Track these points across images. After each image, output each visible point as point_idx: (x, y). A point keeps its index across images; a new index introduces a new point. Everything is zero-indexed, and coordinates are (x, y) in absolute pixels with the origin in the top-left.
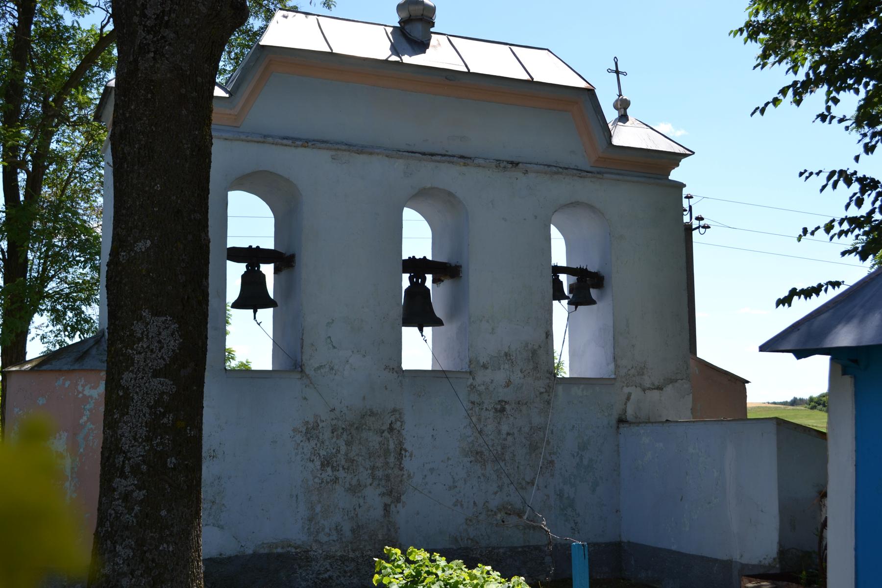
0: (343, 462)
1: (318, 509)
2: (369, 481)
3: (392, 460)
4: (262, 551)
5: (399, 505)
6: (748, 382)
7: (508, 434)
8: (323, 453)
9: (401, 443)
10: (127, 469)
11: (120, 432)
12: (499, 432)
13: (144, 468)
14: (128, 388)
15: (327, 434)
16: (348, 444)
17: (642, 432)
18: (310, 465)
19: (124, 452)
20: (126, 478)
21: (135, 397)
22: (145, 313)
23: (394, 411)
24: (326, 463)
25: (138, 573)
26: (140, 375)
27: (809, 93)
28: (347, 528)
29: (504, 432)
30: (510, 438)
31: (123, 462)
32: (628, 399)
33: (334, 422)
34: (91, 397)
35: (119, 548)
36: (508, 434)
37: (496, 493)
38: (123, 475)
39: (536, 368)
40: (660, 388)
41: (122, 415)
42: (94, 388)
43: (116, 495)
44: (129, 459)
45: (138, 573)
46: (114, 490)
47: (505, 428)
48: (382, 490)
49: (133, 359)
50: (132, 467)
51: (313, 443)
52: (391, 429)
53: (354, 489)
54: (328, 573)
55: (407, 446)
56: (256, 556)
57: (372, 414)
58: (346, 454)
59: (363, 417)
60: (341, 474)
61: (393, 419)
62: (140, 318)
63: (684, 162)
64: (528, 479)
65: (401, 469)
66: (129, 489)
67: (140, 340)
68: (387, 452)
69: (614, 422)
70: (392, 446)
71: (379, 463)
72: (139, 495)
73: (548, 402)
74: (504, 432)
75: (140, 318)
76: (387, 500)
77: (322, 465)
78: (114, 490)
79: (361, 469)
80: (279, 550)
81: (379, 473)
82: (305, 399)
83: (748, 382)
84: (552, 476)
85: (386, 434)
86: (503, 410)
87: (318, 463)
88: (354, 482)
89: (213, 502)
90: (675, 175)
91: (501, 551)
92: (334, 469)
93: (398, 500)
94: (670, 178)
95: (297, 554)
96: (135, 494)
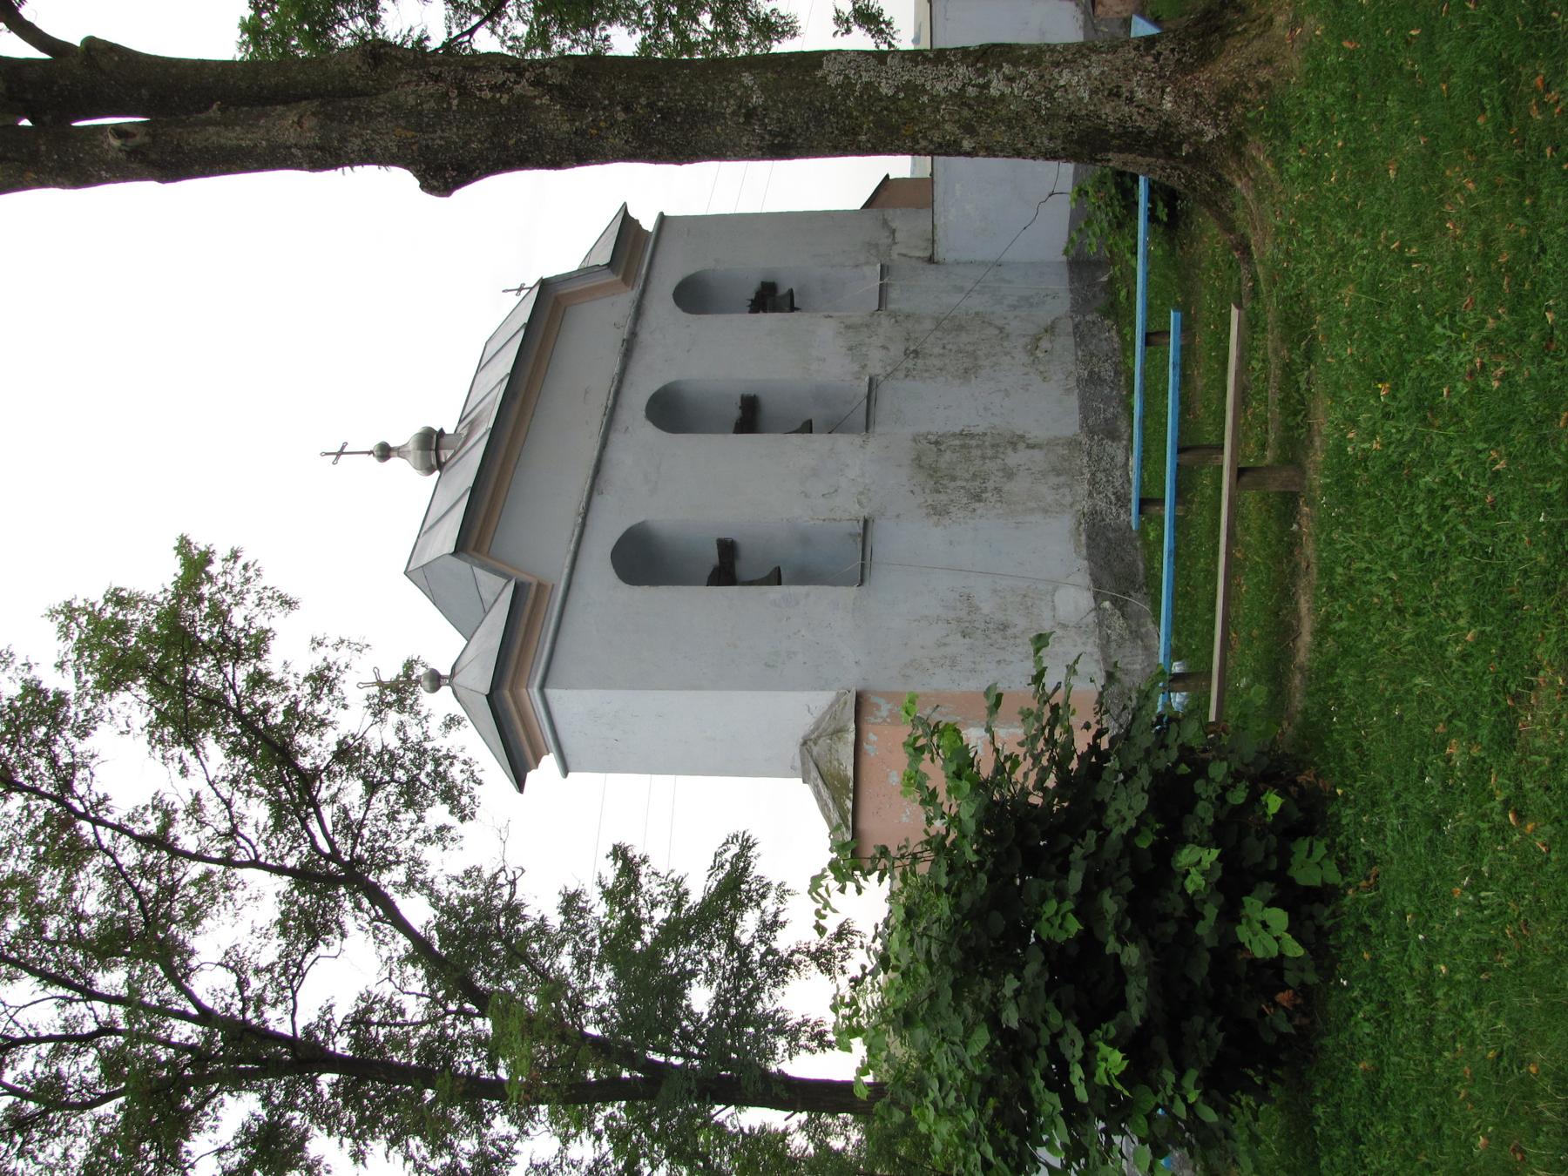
0: (977, 483)
1: (1033, 505)
2: (999, 461)
3: (973, 443)
4: (1084, 552)
5: (1027, 436)
6: (887, 176)
7: (944, 348)
8: (965, 500)
9: (954, 435)
10: (981, 81)
11: (942, 94)
12: (942, 355)
13: (979, 65)
14: (897, 87)
15: (943, 497)
16: (953, 479)
17: (943, 220)
18: (979, 512)
19: (964, 86)
20: (990, 82)
21: (906, 78)
22: (819, 74)
23: (914, 440)
24: (977, 498)
25: (1087, 63)
26: (883, 74)
27: (452, 831)
28: (1054, 480)
29: (941, 351)
30: (949, 347)
31: (973, 86)
32: (905, 255)
33: (927, 491)
34: (890, 711)
35: (1062, 83)
36: (944, 348)
37: (1013, 358)
38: (986, 86)
39: (867, 326)
40: (893, 232)
41: (925, 91)
42: (878, 707)
43: (1008, 91)
44: (971, 79)
45: (1087, 63)
46: (1003, 94)
47: (937, 350)
48: (1009, 451)
49: (867, 83)
50: (979, 76)
51: (952, 509)
52: (937, 443)
53: (1009, 474)
54: (1110, 495)
55: (957, 431)
56: (1090, 558)
57: (918, 458)
58: (967, 481)
59: (921, 467)
60: (990, 485)
61: (924, 442)
62: (824, 78)
63: (633, 213)
64: (997, 332)
65: (985, 434)
66: (1001, 77)
67: (847, 77)
68: (962, 446)
69: (933, 266)
70: (957, 442)
71: (976, 453)
72: (1007, 69)
73: (908, 316)
74: (941, 351)
75: (824, 78)
76: (1021, 446)
77: (980, 501)
78: (1003, 94)
79: (985, 467)
80: (1083, 538)
81: (990, 453)
82: (898, 516)
83: (887, 176)
84: (993, 313)
85: (943, 448)
86: (916, 352)
87: (977, 505)
88: (1001, 474)
89: (1025, 596)
90: (648, 224)
91: (1080, 353)
92: (985, 490)
93: (1022, 437)
94: (650, 229)
95: (1086, 522)
96: (1007, 72)
